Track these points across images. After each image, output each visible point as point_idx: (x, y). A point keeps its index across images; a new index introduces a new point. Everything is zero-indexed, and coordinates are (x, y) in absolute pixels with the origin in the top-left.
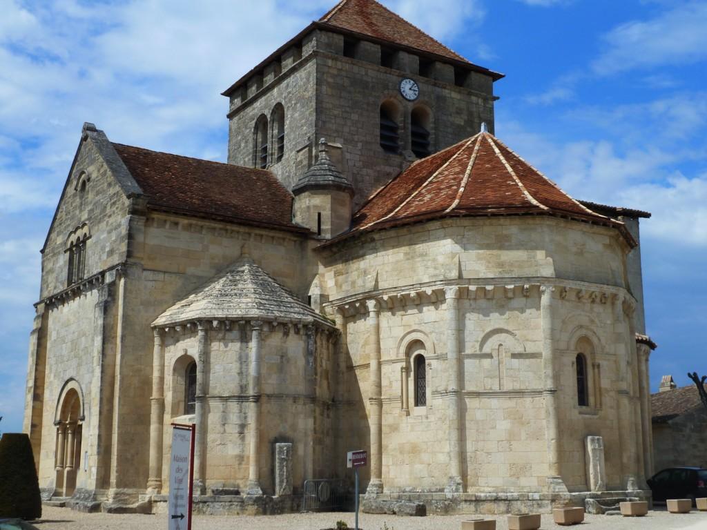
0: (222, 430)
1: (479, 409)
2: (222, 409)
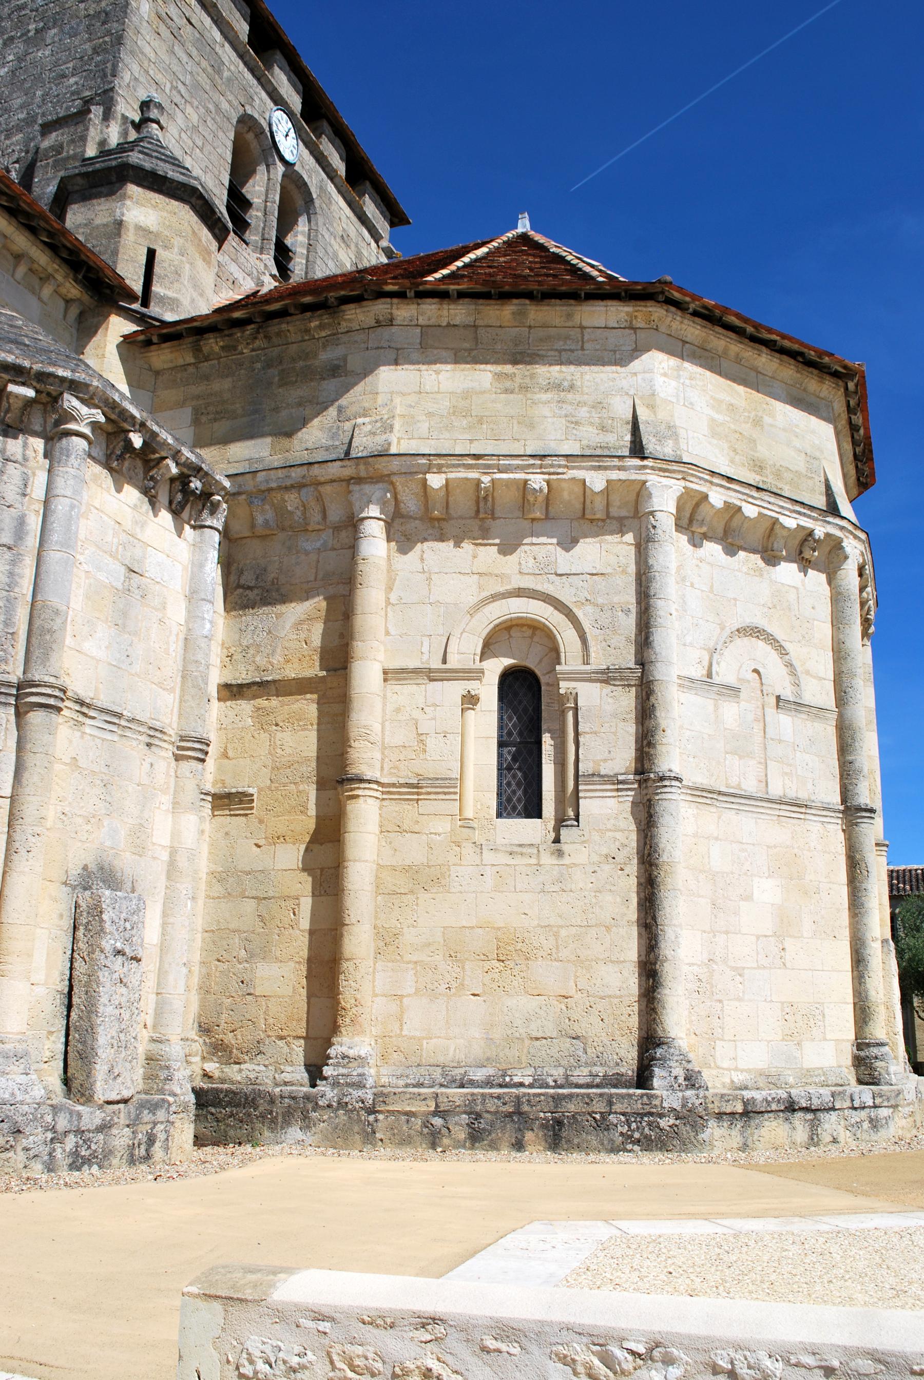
1: (717, 839)
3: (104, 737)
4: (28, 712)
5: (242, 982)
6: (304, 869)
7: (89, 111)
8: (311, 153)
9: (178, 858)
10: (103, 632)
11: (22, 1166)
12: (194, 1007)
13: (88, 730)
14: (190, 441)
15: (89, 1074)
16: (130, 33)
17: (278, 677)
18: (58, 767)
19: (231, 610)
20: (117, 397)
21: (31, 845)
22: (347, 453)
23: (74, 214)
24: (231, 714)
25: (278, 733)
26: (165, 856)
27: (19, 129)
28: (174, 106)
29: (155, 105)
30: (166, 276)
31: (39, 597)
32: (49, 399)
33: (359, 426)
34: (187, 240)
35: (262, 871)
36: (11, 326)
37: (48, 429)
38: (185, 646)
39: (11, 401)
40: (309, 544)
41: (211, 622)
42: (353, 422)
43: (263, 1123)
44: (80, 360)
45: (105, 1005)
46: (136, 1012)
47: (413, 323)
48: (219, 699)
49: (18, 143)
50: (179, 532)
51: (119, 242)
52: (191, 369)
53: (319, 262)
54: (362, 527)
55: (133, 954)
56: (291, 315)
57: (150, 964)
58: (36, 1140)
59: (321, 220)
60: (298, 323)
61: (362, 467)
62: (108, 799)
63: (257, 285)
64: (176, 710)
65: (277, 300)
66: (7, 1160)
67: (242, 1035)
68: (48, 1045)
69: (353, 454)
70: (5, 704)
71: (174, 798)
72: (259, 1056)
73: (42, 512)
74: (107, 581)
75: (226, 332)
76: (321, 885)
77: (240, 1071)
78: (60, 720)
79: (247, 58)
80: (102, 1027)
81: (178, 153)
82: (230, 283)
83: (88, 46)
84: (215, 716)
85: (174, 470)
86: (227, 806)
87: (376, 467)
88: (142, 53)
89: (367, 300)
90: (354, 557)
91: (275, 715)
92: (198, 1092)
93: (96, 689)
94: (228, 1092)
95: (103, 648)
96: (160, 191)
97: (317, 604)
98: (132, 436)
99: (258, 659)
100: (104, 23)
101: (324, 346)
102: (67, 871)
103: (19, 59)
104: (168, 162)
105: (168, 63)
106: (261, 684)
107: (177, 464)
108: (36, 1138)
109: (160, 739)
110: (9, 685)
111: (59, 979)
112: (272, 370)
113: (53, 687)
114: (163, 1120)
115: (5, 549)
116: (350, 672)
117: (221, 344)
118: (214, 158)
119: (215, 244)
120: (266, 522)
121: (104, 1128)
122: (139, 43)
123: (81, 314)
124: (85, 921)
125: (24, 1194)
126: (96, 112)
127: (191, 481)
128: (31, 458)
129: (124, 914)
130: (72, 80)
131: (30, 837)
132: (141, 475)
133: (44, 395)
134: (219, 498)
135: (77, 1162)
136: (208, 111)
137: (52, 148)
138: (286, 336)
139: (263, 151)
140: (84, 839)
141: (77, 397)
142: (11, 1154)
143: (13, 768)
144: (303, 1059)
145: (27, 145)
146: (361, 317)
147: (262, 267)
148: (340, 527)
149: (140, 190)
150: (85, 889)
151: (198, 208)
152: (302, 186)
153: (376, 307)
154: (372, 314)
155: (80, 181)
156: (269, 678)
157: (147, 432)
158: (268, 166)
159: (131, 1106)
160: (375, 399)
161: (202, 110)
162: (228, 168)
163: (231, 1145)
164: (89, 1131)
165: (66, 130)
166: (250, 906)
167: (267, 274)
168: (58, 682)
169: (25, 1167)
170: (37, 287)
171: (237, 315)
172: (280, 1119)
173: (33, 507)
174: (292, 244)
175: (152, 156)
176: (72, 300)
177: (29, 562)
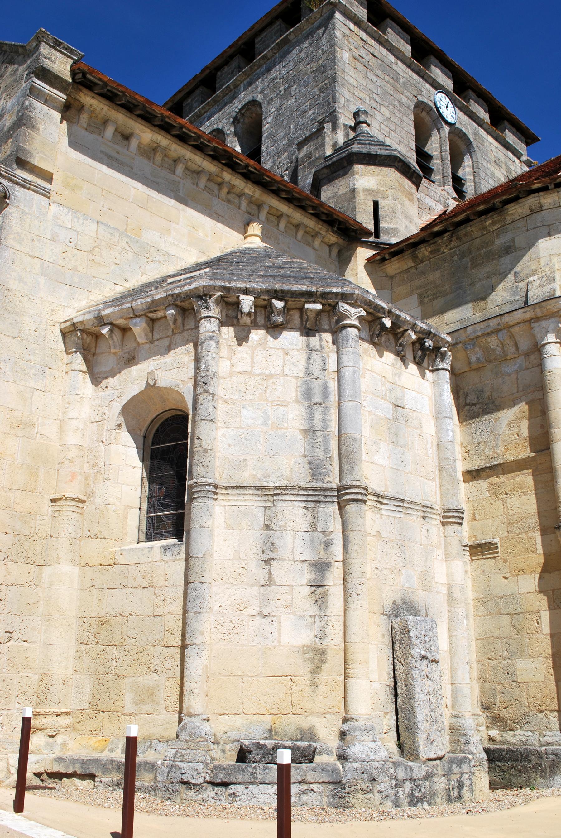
0: (262, 575)
2: (261, 521)
3: (395, 516)
4: (346, 505)
5: (508, 673)
6: (540, 592)
7: (324, 128)
8: (465, 113)
9: (454, 591)
10: (385, 448)
11: (378, 803)
12: (477, 692)
13: (384, 512)
14: (420, 316)
15: (414, 741)
16: (339, 74)
17: (502, 461)
18: (369, 538)
19: (464, 421)
20: (371, 298)
21: (359, 590)
22: (526, 302)
23: (325, 192)
24: (474, 490)
25: (508, 499)
26: (444, 590)
27: (285, 150)
28: (373, 110)
29: (362, 112)
30: (387, 215)
31: (343, 432)
32: (330, 308)
33: (531, 283)
34: (396, 190)
35: (511, 595)
36: (301, 268)
37: (333, 327)
38: (438, 449)
39: (308, 314)
40: (509, 368)
41: (453, 431)
42: (526, 281)
43: (536, 773)
44: (345, 280)
45: (419, 694)
46: (440, 697)
47: (557, 205)
48: (465, 482)
49: (285, 159)
50: (423, 376)
51: (355, 202)
52: (413, 270)
53: (482, 182)
54: (544, 350)
55: (432, 658)
56: (472, 220)
57: (445, 664)
58: (385, 786)
59: (479, 154)
60: (477, 224)
61: (538, 310)
62: (403, 556)
63: (445, 207)
64: (438, 492)
65: (461, 213)
66: (369, 799)
67: (513, 710)
68: (385, 721)
69: (530, 302)
70: (332, 502)
71: (445, 551)
72: (526, 725)
73: (336, 378)
74: (382, 415)
75: (432, 242)
76: (554, 602)
77: (515, 736)
78: (366, 508)
79: (413, 66)
80: (419, 709)
81: (381, 138)
82: (427, 210)
83: (316, 90)
84: (464, 493)
85: (414, 337)
86: (481, 553)
87: (548, 308)
88: (349, 83)
89: (522, 198)
90: (542, 372)
91: (504, 487)
92: (488, 751)
93: (386, 485)
94: (508, 751)
95: (386, 458)
96: (374, 164)
97: (522, 408)
98: (384, 320)
99: (486, 451)
100: (323, 73)
101: (498, 235)
102: (383, 606)
103: (278, 110)
104: (376, 145)
105: (365, 85)
106: (492, 468)
107: (415, 332)
108: (385, 784)
109: (431, 513)
110: (332, 490)
111: (387, 678)
112: (465, 259)
113: (360, 488)
114: (467, 771)
115: (318, 405)
116: (553, 450)
117: (429, 250)
118: (404, 134)
119: (414, 188)
120: (478, 359)
121: (428, 777)
122: (346, 78)
123: (340, 253)
124: (399, 638)
125: (383, 822)
126: (328, 127)
127: (425, 342)
128: (325, 347)
129: (424, 632)
130: (310, 112)
131: (358, 585)
132: (394, 344)
133: (327, 306)
134: (446, 349)
135: (414, 801)
136: (395, 106)
137: (305, 156)
138: (471, 235)
139: (433, 121)
140: (391, 583)
141: (347, 303)
142: (371, 795)
143: (342, 542)
144: (558, 726)
145: (291, 159)
146: (520, 210)
147: (446, 194)
148: (529, 353)
149: (362, 166)
150: (396, 617)
151: (400, 168)
152: (462, 136)
153: (529, 201)
154: (527, 206)
155: (325, 171)
156: (497, 463)
157: (393, 316)
158: (438, 130)
159: (445, 762)
160: (539, 262)
161: (391, 107)
162: (413, 138)
163: (515, 789)
164: (419, 779)
165: (312, 143)
166: (506, 620)
167: (450, 198)
168: (362, 484)
169: (381, 804)
170: (311, 242)
171: (436, 229)
172: (548, 770)
173: (331, 376)
174: (463, 175)
175: (366, 144)
176: (332, 244)
177: (334, 411)
